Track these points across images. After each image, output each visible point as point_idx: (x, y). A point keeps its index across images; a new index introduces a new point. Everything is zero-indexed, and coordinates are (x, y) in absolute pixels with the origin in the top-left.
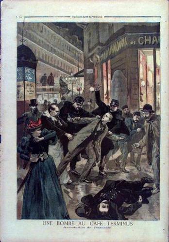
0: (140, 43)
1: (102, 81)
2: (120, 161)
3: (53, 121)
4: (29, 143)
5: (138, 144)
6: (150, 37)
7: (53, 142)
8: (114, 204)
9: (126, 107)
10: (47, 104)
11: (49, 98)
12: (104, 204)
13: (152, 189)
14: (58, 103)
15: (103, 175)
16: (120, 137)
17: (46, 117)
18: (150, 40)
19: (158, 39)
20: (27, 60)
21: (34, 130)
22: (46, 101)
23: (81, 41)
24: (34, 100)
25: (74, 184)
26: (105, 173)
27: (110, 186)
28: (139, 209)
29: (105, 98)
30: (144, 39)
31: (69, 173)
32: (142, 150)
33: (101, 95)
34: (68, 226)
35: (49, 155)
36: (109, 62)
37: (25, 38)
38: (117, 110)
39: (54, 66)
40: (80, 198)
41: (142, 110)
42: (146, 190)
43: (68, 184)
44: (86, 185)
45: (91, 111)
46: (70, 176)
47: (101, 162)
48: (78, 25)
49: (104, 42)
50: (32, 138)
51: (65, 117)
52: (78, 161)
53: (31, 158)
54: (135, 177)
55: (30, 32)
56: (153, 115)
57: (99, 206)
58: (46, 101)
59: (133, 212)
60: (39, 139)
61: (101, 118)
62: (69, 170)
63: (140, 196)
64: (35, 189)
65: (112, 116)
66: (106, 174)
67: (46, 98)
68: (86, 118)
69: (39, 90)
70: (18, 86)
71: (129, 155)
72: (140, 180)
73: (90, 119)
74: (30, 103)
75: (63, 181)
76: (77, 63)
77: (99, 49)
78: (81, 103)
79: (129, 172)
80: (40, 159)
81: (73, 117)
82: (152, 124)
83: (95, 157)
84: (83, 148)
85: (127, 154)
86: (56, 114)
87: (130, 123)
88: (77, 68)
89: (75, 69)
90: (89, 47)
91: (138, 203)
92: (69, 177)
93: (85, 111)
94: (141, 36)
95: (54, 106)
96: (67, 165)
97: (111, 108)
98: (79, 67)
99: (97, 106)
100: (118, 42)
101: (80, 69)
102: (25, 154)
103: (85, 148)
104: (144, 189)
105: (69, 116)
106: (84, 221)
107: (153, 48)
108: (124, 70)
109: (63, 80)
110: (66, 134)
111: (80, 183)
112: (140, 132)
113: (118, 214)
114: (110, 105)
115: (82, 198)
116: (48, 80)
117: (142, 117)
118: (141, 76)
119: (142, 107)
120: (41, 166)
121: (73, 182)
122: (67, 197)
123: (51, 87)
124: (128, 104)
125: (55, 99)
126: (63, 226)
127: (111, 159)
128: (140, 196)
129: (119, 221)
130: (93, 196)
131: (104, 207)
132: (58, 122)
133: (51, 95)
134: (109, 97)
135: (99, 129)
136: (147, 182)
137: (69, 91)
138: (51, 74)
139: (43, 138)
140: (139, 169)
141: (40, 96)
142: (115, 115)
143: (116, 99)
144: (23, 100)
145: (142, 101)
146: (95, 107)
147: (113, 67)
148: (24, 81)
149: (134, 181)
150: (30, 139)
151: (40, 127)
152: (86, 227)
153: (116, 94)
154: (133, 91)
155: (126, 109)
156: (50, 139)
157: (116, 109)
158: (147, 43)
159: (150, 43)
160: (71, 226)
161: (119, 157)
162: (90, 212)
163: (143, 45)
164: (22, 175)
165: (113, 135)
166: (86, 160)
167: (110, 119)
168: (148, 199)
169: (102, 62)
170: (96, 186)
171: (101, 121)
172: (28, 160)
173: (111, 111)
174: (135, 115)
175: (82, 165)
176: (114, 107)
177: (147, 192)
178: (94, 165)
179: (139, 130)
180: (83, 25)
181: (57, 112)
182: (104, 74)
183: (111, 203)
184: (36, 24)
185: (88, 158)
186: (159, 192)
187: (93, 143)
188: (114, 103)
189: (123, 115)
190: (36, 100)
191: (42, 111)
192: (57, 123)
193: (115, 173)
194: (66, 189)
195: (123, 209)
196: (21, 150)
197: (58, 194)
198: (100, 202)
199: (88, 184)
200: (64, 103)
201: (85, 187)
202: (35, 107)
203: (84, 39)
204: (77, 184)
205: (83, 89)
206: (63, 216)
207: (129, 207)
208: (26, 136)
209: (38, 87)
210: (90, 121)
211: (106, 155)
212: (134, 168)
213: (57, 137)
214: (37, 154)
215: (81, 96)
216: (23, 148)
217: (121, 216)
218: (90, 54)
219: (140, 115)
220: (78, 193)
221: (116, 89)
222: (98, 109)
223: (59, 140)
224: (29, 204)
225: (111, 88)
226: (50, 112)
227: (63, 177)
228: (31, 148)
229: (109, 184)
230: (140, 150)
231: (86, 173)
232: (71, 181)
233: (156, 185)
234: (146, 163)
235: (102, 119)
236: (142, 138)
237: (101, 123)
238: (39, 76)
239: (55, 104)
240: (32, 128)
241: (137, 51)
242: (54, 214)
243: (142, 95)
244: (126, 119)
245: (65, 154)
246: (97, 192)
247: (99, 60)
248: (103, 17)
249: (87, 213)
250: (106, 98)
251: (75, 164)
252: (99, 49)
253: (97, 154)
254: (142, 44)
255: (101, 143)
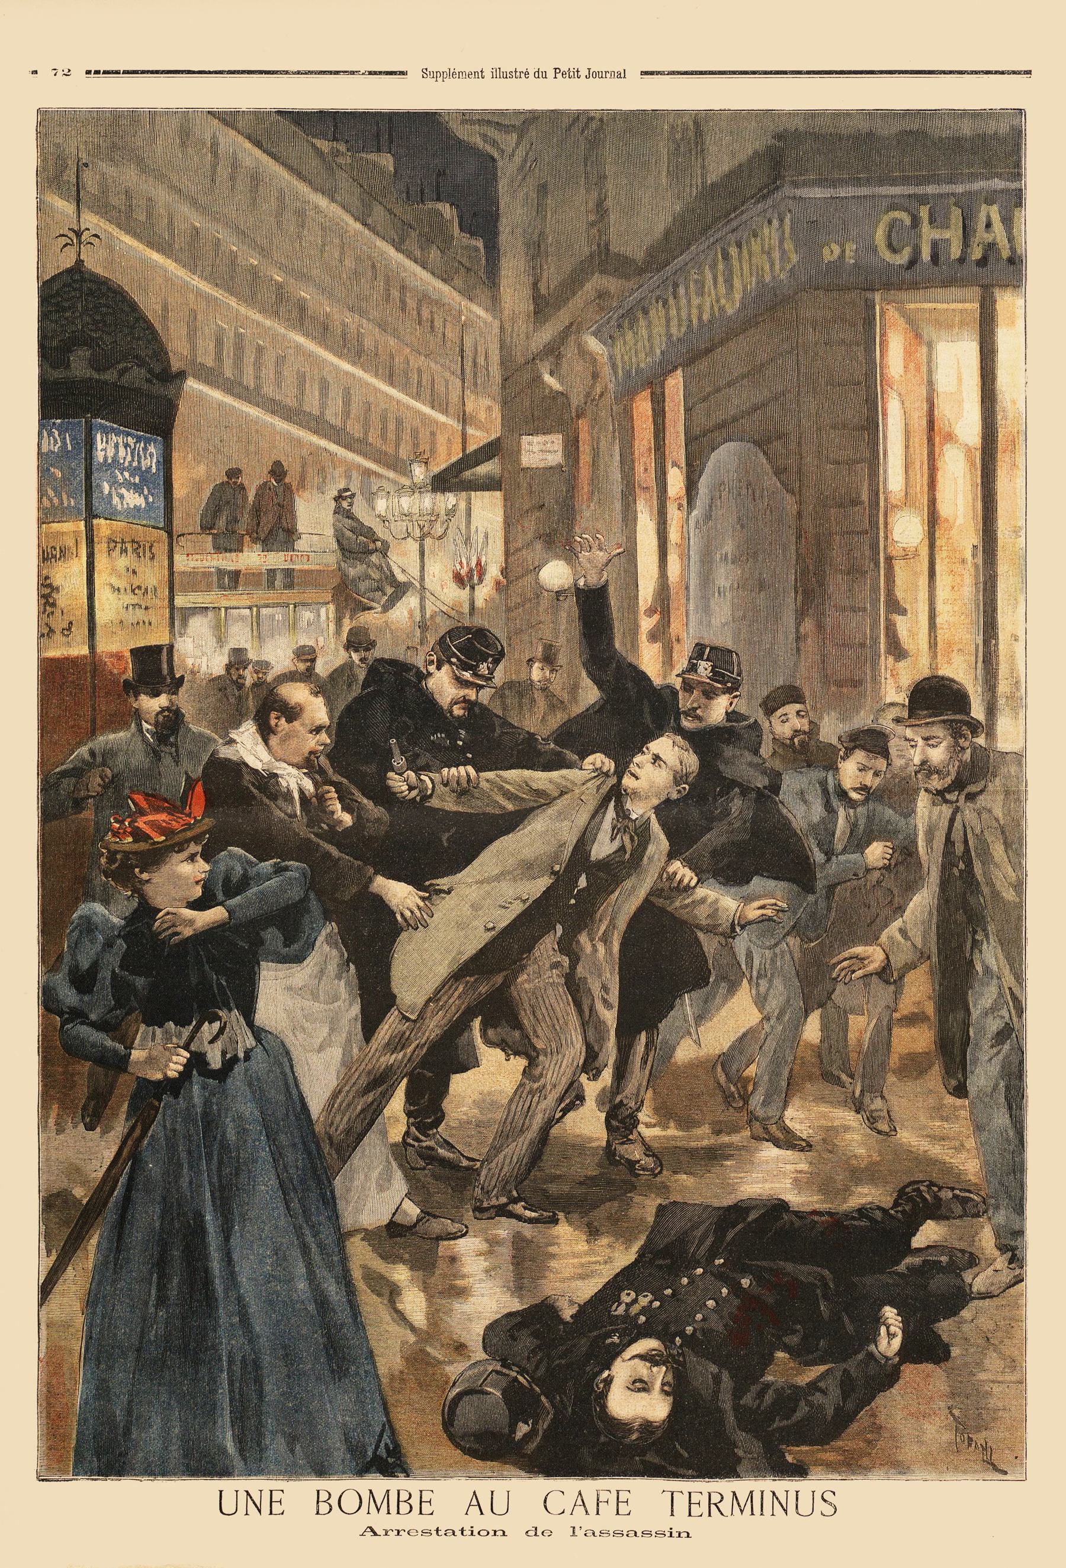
0: (887, 255)
1: (629, 519)
2: (752, 1071)
3: (288, 796)
4: (121, 945)
5: (875, 956)
6: (956, 214)
7: (288, 942)
8: (713, 1368)
9: (792, 694)
10: (249, 677)
11: (259, 637)
12: (642, 1369)
13: (974, 1261)
14: (322, 668)
15: (631, 1164)
16: (747, 899)
17: (238, 767)
18: (953, 235)
19: (1008, 221)
20: (110, 376)
21: (154, 858)
22: (238, 660)
23: (480, 244)
24: (158, 648)
25: (436, 1226)
26: (649, 1151)
27: (682, 1240)
28: (880, 1400)
29: (643, 637)
30: (916, 222)
31: (400, 1151)
32: (898, 994)
33: (615, 614)
34: (394, 1521)
35: (258, 1033)
36: (675, 384)
37: (91, 221)
38: (731, 716)
39: (290, 414)
40: (478, 1329)
41: (898, 721)
42: (929, 1268)
43: (394, 1229)
44: (519, 1243)
45: (556, 720)
46: (408, 1178)
47: (621, 1073)
48: (462, 132)
49: (635, 249)
50: (146, 911)
51: (370, 769)
52: (464, 1068)
53: (136, 1054)
54: (858, 1174)
55: (130, 176)
56: (975, 748)
57: (608, 1382)
58: (238, 660)
59: (842, 1420)
60: (191, 922)
61: (620, 773)
62: (396, 1133)
63: (890, 1313)
64: (161, 1265)
65: (692, 761)
66: (649, 1162)
67: (240, 636)
68: (513, 774)
69: (197, 581)
70: (48, 556)
71: (812, 1030)
72: (887, 1201)
73: (540, 779)
74: (129, 675)
75: (358, 1211)
76: (454, 397)
77: (602, 295)
78: (483, 669)
79: (805, 1146)
80: (198, 1061)
81: (427, 768)
82: (968, 814)
83: (575, 1050)
84: (499, 979)
85: (797, 1026)
86: (312, 742)
87: (817, 811)
88: (454, 424)
89: (441, 439)
90: (535, 285)
91: (871, 1356)
92: (399, 1186)
93: (505, 723)
94: (892, 207)
95: (297, 693)
96: (386, 1096)
97: (685, 702)
98: (464, 419)
99: (590, 694)
100: (733, 251)
101: (478, 438)
102: (93, 1025)
103: (506, 984)
104: (917, 1260)
105: (398, 761)
106: (499, 1486)
107: (976, 292)
108: (777, 445)
109: (359, 509)
110: (584, 876)
111: (475, 1225)
112: (887, 868)
113: (541, 1433)
114: (678, 683)
115: (490, 1328)
116: (257, 511)
117: (898, 763)
118: (894, 479)
119: (902, 698)
120: (207, 1103)
121: (427, 1214)
122: (386, 1315)
123: (276, 560)
124: (808, 682)
125: (304, 640)
126: (363, 1520)
127: (685, 1052)
128: (890, 1313)
129: (742, 1486)
130: (568, 1313)
131: (640, 1386)
132: (321, 798)
133: (279, 614)
134: (676, 627)
135: (603, 848)
136: (935, 1211)
137: (401, 590)
138: (278, 471)
139: (216, 914)
140: (883, 1126)
141: (199, 625)
142: (718, 755)
143: (726, 641)
144: (85, 651)
145: (897, 651)
146: (574, 698)
147: (702, 420)
148: (91, 515)
149: (853, 1202)
150: (132, 919)
151: (196, 839)
152: (515, 1524)
153: (722, 611)
154: (837, 585)
155: (792, 709)
156: (268, 920)
157: (718, 710)
158: (935, 258)
159: (956, 252)
160: (414, 1521)
161: (744, 1035)
162: (544, 1425)
163: (913, 263)
164: (75, 1171)
165: (701, 892)
166: (519, 1063)
167: (678, 779)
168: (944, 1327)
169: (627, 394)
170: (582, 1247)
171: (616, 795)
172: (121, 1063)
173: (687, 724)
174: (849, 752)
175: (485, 1103)
176: (709, 694)
177: (938, 1283)
178: (573, 1098)
179: (876, 852)
180: (492, 133)
181: (318, 730)
182: (639, 469)
183: (692, 1358)
184: (175, 122)
185: (525, 1049)
186: (1019, 1280)
187: (568, 946)
188: (704, 668)
189: (766, 750)
190: (171, 648)
191: (213, 725)
192: (313, 806)
193: (713, 1156)
194: (378, 1265)
195: (769, 1398)
196: (69, 996)
197: (322, 1303)
198: (615, 1352)
199: (527, 1230)
200: (362, 675)
201: (505, 1252)
202: (163, 700)
203: (505, 226)
204: (453, 1227)
205: (493, 571)
206: (355, 1449)
207: (813, 1386)
208: (106, 902)
209: (181, 562)
210: (539, 793)
211: (652, 1027)
212: (848, 1117)
213: (314, 904)
214: (182, 1023)
215: (478, 622)
216: (83, 981)
217: (757, 1447)
218: (546, 335)
219: (885, 753)
220: (462, 1293)
221: (724, 576)
222: (599, 709)
223: (331, 927)
224: (121, 1377)
225: (686, 568)
226: (265, 731)
227: (359, 1179)
228: (140, 982)
229: (677, 1225)
230: (883, 993)
231: (519, 1148)
232: (412, 1210)
233: (997, 1235)
234: (935, 1077)
235: (627, 781)
236: (900, 910)
237: (622, 813)
238: (198, 485)
239: (308, 676)
240: (143, 846)
241: (870, 306)
242: (292, 1440)
243: (904, 612)
244: (792, 782)
245: (370, 1025)
246: (587, 1289)
247: (607, 371)
248: (414, 74)
249: (523, 1429)
250: (653, 637)
251: (443, 1089)
252: (602, 295)
253: (589, 1021)
254: (902, 258)
255: (616, 947)
